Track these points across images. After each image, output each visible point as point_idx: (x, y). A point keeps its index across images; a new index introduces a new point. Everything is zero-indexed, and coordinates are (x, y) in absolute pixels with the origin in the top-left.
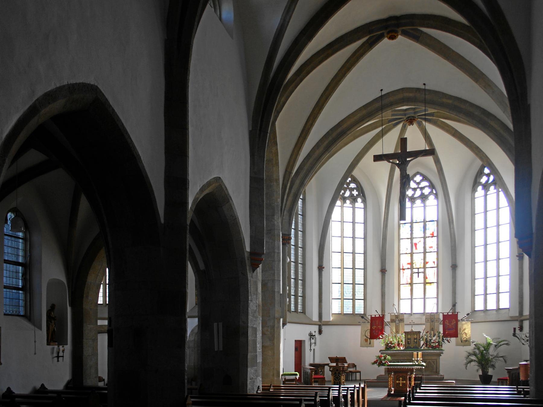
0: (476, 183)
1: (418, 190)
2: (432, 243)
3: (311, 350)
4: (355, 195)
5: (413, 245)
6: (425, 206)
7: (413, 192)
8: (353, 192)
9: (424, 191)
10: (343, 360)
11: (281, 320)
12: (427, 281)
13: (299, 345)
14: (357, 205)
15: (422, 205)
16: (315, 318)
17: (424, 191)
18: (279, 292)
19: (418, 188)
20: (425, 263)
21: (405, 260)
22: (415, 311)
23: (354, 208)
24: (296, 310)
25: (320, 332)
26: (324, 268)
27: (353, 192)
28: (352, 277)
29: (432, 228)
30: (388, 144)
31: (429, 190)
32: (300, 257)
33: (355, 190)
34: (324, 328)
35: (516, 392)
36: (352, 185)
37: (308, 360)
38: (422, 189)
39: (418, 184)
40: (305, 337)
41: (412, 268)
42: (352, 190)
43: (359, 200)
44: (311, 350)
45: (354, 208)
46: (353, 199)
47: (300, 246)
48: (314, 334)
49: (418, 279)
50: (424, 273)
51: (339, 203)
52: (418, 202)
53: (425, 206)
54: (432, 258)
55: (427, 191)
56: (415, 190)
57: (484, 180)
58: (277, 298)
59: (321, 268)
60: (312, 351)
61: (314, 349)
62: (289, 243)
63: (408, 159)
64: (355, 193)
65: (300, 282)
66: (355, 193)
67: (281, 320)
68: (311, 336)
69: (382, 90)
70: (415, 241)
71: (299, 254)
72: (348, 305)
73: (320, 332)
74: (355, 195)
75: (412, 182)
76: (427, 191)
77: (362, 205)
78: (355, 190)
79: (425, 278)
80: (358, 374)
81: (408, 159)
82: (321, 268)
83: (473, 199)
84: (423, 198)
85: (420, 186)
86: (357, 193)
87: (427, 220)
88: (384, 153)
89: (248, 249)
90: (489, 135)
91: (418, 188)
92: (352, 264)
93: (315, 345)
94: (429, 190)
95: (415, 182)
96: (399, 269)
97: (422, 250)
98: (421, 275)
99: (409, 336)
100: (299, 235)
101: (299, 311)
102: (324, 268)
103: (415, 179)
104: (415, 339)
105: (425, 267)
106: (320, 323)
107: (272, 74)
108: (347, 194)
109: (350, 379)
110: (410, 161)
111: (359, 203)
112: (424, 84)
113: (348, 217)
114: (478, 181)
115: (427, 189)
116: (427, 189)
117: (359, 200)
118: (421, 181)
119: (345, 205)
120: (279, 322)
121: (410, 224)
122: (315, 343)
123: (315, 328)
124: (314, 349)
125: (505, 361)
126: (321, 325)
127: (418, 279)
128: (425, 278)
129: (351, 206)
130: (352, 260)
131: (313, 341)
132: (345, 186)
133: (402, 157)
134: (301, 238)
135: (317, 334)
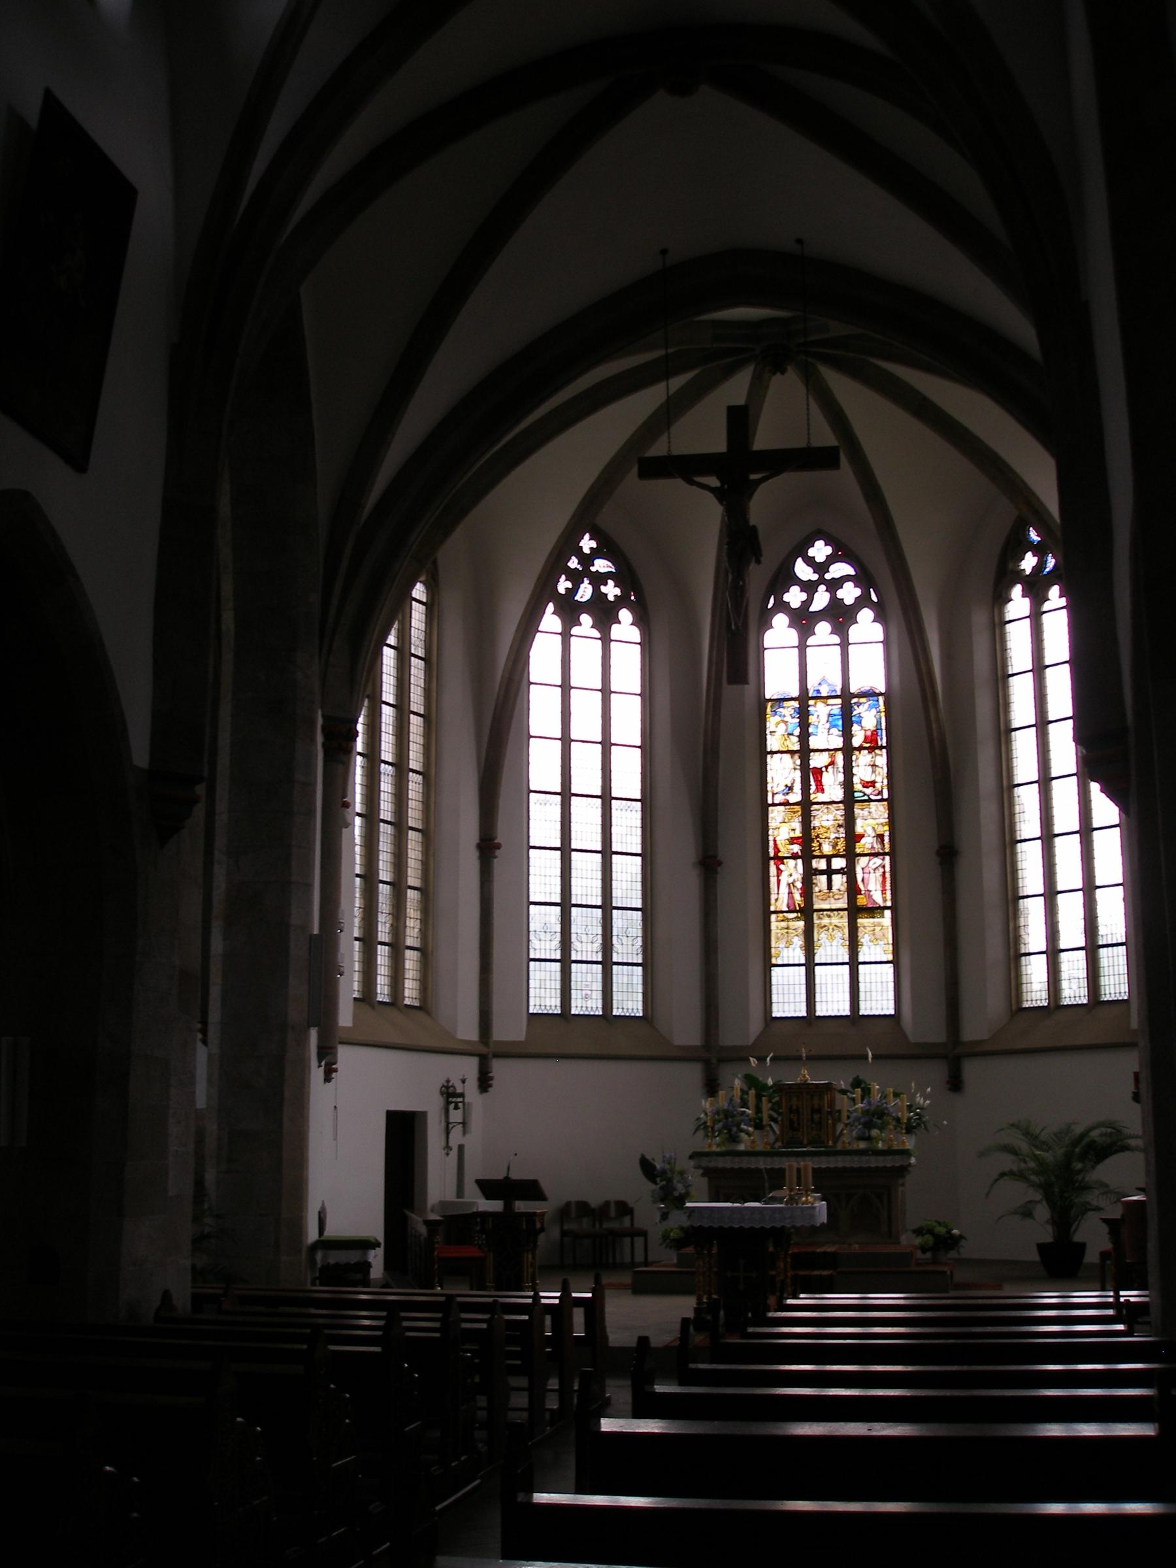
0: (1005, 577)
1: (822, 588)
2: (871, 768)
3: (448, 1147)
4: (611, 598)
5: (810, 775)
6: (844, 645)
7: (804, 596)
8: (603, 589)
9: (840, 594)
10: (531, 1190)
11: (314, 1034)
12: (861, 901)
13: (403, 1131)
14: (616, 631)
15: (836, 639)
16: (468, 1031)
17: (840, 594)
18: (305, 926)
19: (822, 580)
20: (853, 838)
21: (783, 828)
22: (821, 1010)
23: (606, 640)
24: (367, 997)
25: (484, 1083)
26: (498, 846)
27: (603, 589)
28: (599, 884)
29: (869, 717)
30: (703, 432)
31: (857, 592)
32: (412, 804)
33: (611, 583)
34: (498, 1068)
35: (1111, 1312)
36: (601, 565)
37: (439, 1184)
38: (834, 585)
39: (821, 568)
40: (429, 1104)
41: (807, 855)
42: (599, 580)
43: (625, 615)
44: (448, 1147)
45: (606, 640)
46: (604, 615)
47: (413, 765)
48: (459, 1090)
49: (831, 895)
50: (849, 872)
51: (550, 621)
52: (823, 629)
53: (844, 645)
54: (872, 821)
55: (849, 593)
56: (810, 588)
57: (1029, 562)
58: (298, 950)
59: (487, 847)
60: (454, 1153)
61: (461, 1148)
62: (349, 750)
63: (753, 477)
64: (611, 590)
65: (384, 890)
66: (611, 590)
67: (314, 1034)
68: (450, 1095)
69: (664, 252)
70: (817, 761)
71: (411, 795)
72: (587, 980)
73: (484, 1083)
74: (611, 598)
75: (799, 562)
76: (849, 593)
77: (635, 634)
78: (611, 583)
79: (853, 889)
80: (639, 1241)
81: (753, 477)
82: (487, 847)
83: (998, 625)
84: (840, 616)
85: (828, 576)
86: (618, 591)
87: (854, 689)
88: (675, 452)
89: (140, 756)
90: (1010, 412)
91: (822, 580)
92: (599, 837)
93: (464, 1133)
94: (857, 592)
95: (810, 562)
96: (766, 859)
97: (838, 794)
98: (839, 881)
99: (794, 1102)
100: (413, 729)
101: (407, 1002)
102: (498, 846)
103: (811, 552)
104: (813, 1111)
105: (851, 856)
106: (483, 1049)
107: (259, 167)
108: (585, 592)
109: (628, 1259)
110: (759, 482)
111: (625, 628)
112: (799, 241)
113: (586, 670)
114: (1011, 566)
115: (849, 586)
116: (849, 586)
117: (625, 615)
118: (831, 560)
119: (575, 630)
120: (303, 1041)
121: (796, 704)
122: (464, 1123)
123: (469, 1067)
124: (461, 1148)
125: (987, 1195)
126: (487, 1054)
127: (831, 895)
128: (853, 889)
129: (597, 634)
130: (599, 820)
131: (456, 1116)
132: (573, 563)
133: (736, 471)
134: (420, 740)
135: (471, 1090)
